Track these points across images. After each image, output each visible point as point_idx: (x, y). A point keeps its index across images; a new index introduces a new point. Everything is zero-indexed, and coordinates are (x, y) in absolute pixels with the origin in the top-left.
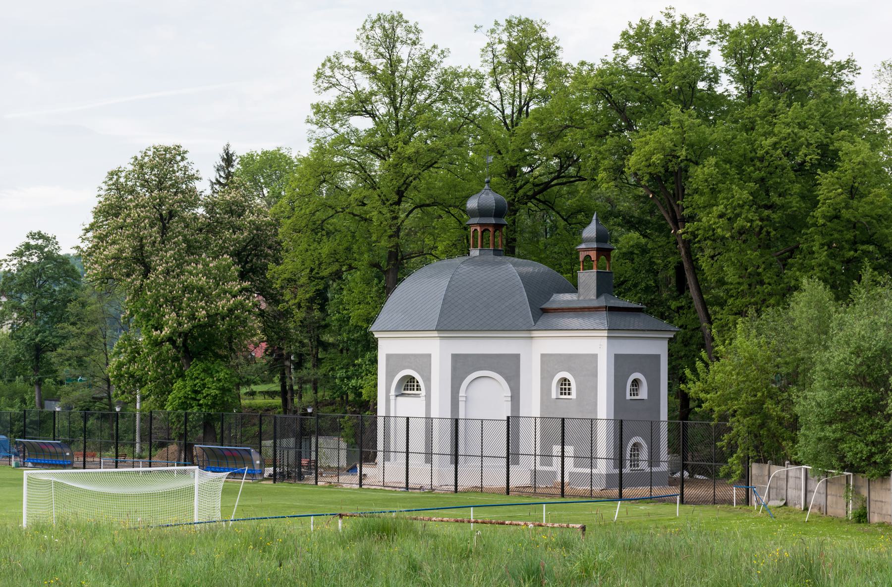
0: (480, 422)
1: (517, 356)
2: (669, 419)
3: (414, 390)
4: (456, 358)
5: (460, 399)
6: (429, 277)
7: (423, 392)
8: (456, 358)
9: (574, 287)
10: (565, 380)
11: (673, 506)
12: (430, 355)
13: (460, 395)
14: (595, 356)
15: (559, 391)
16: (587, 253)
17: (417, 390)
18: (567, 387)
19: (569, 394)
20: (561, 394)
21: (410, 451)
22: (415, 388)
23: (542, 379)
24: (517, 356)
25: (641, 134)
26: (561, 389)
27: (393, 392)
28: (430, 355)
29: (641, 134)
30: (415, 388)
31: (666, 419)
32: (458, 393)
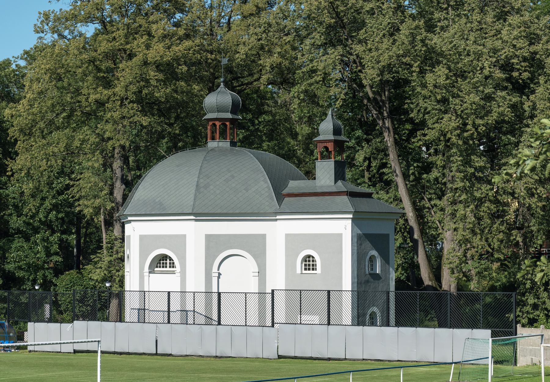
0: (244, 295)
1: (263, 237)
2: (396, 290)
3: (166, 267)
4: (209, 238)
5: (213, 275)
6: (178, 166)
7: (178, 269)
8: (209, 238)
9: (310, 174)
10: (309, 256)
11: (547, 365)
12: (185, 236)
13: (213, 271)
14: (340, 236)
15: (303, 267)
16: (325, 144)
17: (313, 269)
18: (311, 263)
19: (316, 270)
20: (305, 269)
21: (275, 321)
22: (168, 265)
23: (287, 256)
24: (263, 237)
25: (39, 20)
26: (305, 265)
27: (146, 269)
28: (185, 236)
29: (39, 20)
30: (168, 265)
31: (394, 290)
32: (212, 269)
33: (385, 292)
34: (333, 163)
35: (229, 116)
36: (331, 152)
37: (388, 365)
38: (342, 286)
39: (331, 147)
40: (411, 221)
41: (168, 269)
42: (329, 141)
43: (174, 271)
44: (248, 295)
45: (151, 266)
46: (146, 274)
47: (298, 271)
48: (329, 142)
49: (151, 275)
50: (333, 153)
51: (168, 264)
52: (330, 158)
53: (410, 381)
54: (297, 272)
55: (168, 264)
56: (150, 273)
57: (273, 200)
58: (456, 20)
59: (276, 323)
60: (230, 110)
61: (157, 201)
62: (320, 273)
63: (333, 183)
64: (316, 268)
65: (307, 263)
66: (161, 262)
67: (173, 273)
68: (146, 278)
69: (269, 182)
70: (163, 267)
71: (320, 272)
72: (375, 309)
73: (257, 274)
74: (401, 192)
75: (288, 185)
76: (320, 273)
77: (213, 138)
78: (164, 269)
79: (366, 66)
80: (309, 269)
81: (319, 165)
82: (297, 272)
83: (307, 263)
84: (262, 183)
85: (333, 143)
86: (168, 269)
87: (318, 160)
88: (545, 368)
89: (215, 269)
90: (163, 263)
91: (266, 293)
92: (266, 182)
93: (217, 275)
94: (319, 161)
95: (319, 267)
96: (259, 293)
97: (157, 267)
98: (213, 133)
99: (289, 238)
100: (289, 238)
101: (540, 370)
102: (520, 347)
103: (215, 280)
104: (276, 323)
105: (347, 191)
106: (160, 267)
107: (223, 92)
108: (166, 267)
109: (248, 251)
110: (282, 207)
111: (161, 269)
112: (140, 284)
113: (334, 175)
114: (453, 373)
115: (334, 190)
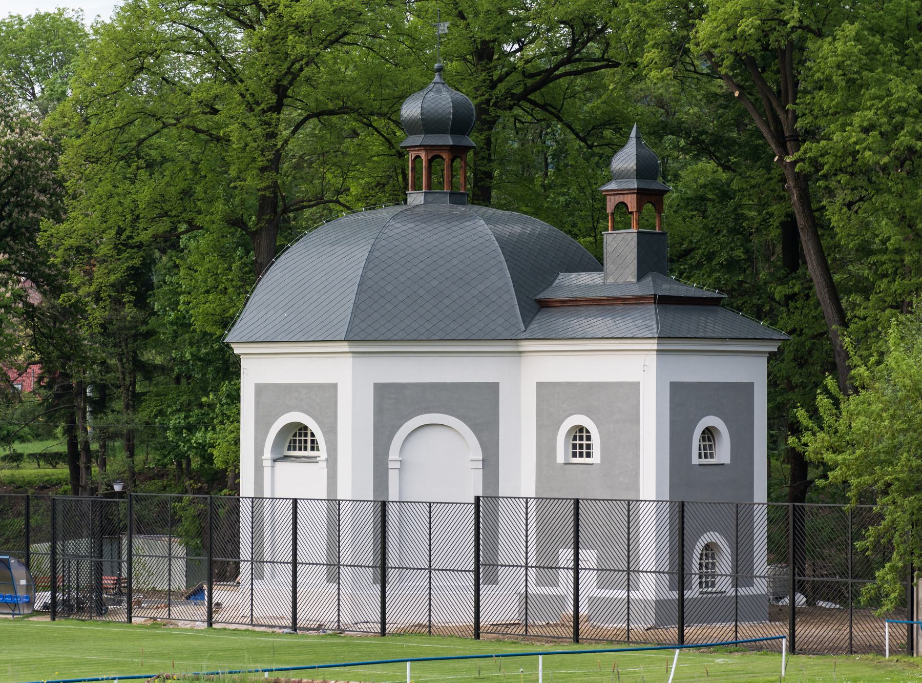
1: (493, 388)
3: (306, 449)
4: (382, 390)
5: (391, 465)
7: (322, 453)
8: (382, 390)
9: (596, 262)
10: (581, 429)
13: (390, 458)
14: (635, 386)
15: (571, 450)
17: (313, 449)
18: (585, 442)
20: (574, 455)
21: (299, 560)
23: (539, 427)
24: (493, 388)
26: (574, 446)
27: (267, 454)
33: (572, 501)
34: (634, 237)
37: (288, 663)
38: (637, 490)
42: (629, 192)
43: (316, 457)
46: (267, 464)
47: (560, 458)
51: (309, 442)
52: (628, 226)
54: (558, 461)
55: (309, 442)
59: (300, 563)
63: (633, 279)
64: (318, 447)
65: (578, 442)
66: (297, 438)
70: (300, 449)
71: (599, 462)
73: (480, 465)
80: (581, 455)
81: (609, 241)
82: (558, 461)
83: (578, 442)
85: (635, 196)
90: (300, 441)
91: (263, 498)
94: (610, 232)
104: (300, 563)
105: (655, 295)
108: (306, 449)
109: (289, 409)
114: (673, 679)
115: (636, 291)
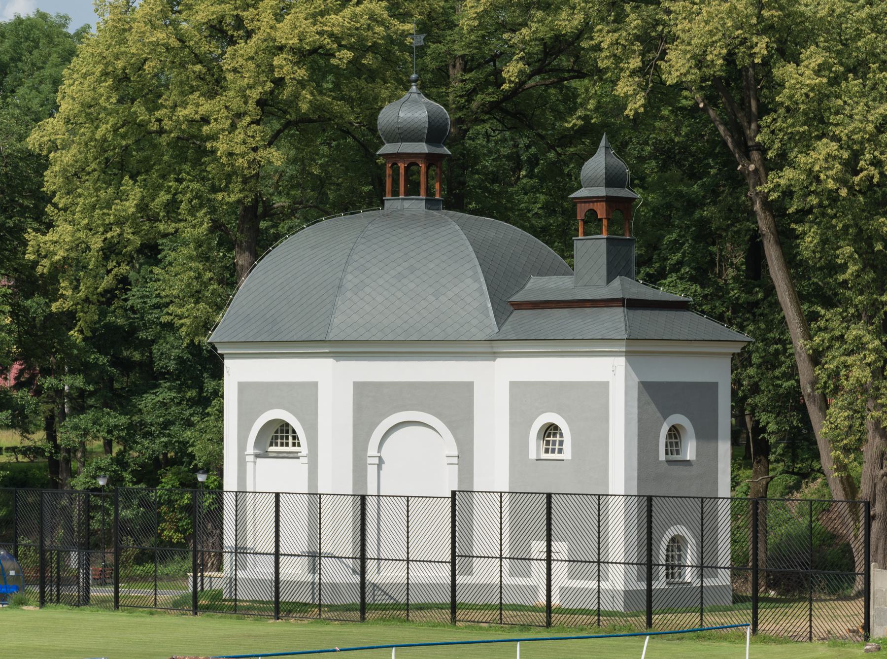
1: (469, 387)
4: (361, 389)
5: (370, 461)
7: (304, 449)
8: (361, 389)
12: (315, 385)
13: (369, 454)
14: (605, 385)
23: (513, 424)
24: (469, 387)
27: (250, 449)
32: (366, 450)
34: (603, 245)
35: (423, 148)
36: (601, 220)
39: (601, 210)
40: (800, 357)
41: (291, 448)
42: (598, 199)
43: (297, 453)
44: (411, 500)
45: (258, 443)
46: (250, 459)
48: (596, 202)
49: (259, 460)
50: (605, 222)
53: (258, 656)
54: (530, 457)
56: (257, 456)
57: (488, 316)
58: (112, 100)
60: (425, 136)
61: (268, 316)
62: (570, 458)
67: (294, 456)
68: (250, 467)
69: (482, 279)
70: (282, 445)
72: (681, 530)
73: (455, 460)
74: (782, 297)
75: (525, 285)
76: (570, 458)
77: (395, 193)
78: (284, 449)
79: (688, 56)
80: (553, 451)
82: (530, 457)
84: (469, 281)
85: (604, 204)
86: (291, 448)
87: (578, 236)
88: (746, 644)
89: (372, 450)
91: (607, 495)
92: (477, 280)
93: (376, 461)
95: (567, 446)
96: (509, 493)
97: (271, 445)
98: (395, 182)
99: (517, 389)
100: (517, 389)
101: (650, 645)
102: (876, 607)
103: (372, 471)
106: (276, 445)
107: (416, 102)
108: (287, 445)
110: (504, 328)
111: (279, 449)
112: (239, 478)
113: (605, 267)
